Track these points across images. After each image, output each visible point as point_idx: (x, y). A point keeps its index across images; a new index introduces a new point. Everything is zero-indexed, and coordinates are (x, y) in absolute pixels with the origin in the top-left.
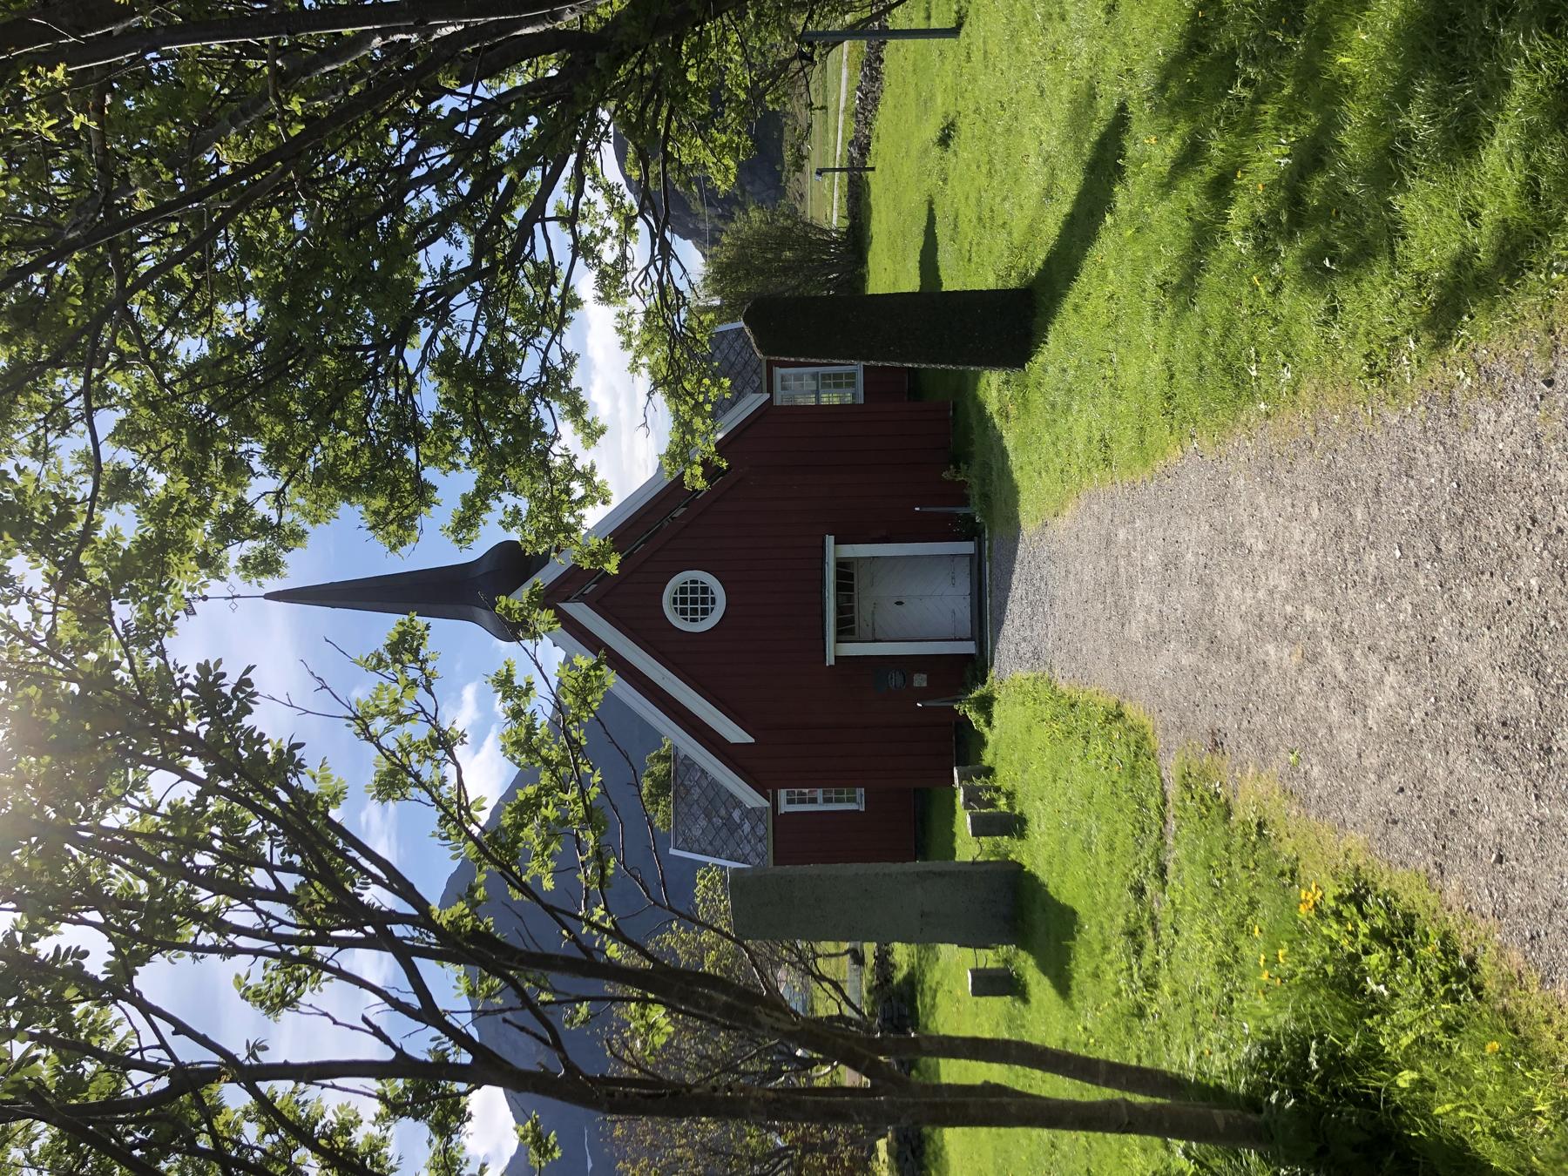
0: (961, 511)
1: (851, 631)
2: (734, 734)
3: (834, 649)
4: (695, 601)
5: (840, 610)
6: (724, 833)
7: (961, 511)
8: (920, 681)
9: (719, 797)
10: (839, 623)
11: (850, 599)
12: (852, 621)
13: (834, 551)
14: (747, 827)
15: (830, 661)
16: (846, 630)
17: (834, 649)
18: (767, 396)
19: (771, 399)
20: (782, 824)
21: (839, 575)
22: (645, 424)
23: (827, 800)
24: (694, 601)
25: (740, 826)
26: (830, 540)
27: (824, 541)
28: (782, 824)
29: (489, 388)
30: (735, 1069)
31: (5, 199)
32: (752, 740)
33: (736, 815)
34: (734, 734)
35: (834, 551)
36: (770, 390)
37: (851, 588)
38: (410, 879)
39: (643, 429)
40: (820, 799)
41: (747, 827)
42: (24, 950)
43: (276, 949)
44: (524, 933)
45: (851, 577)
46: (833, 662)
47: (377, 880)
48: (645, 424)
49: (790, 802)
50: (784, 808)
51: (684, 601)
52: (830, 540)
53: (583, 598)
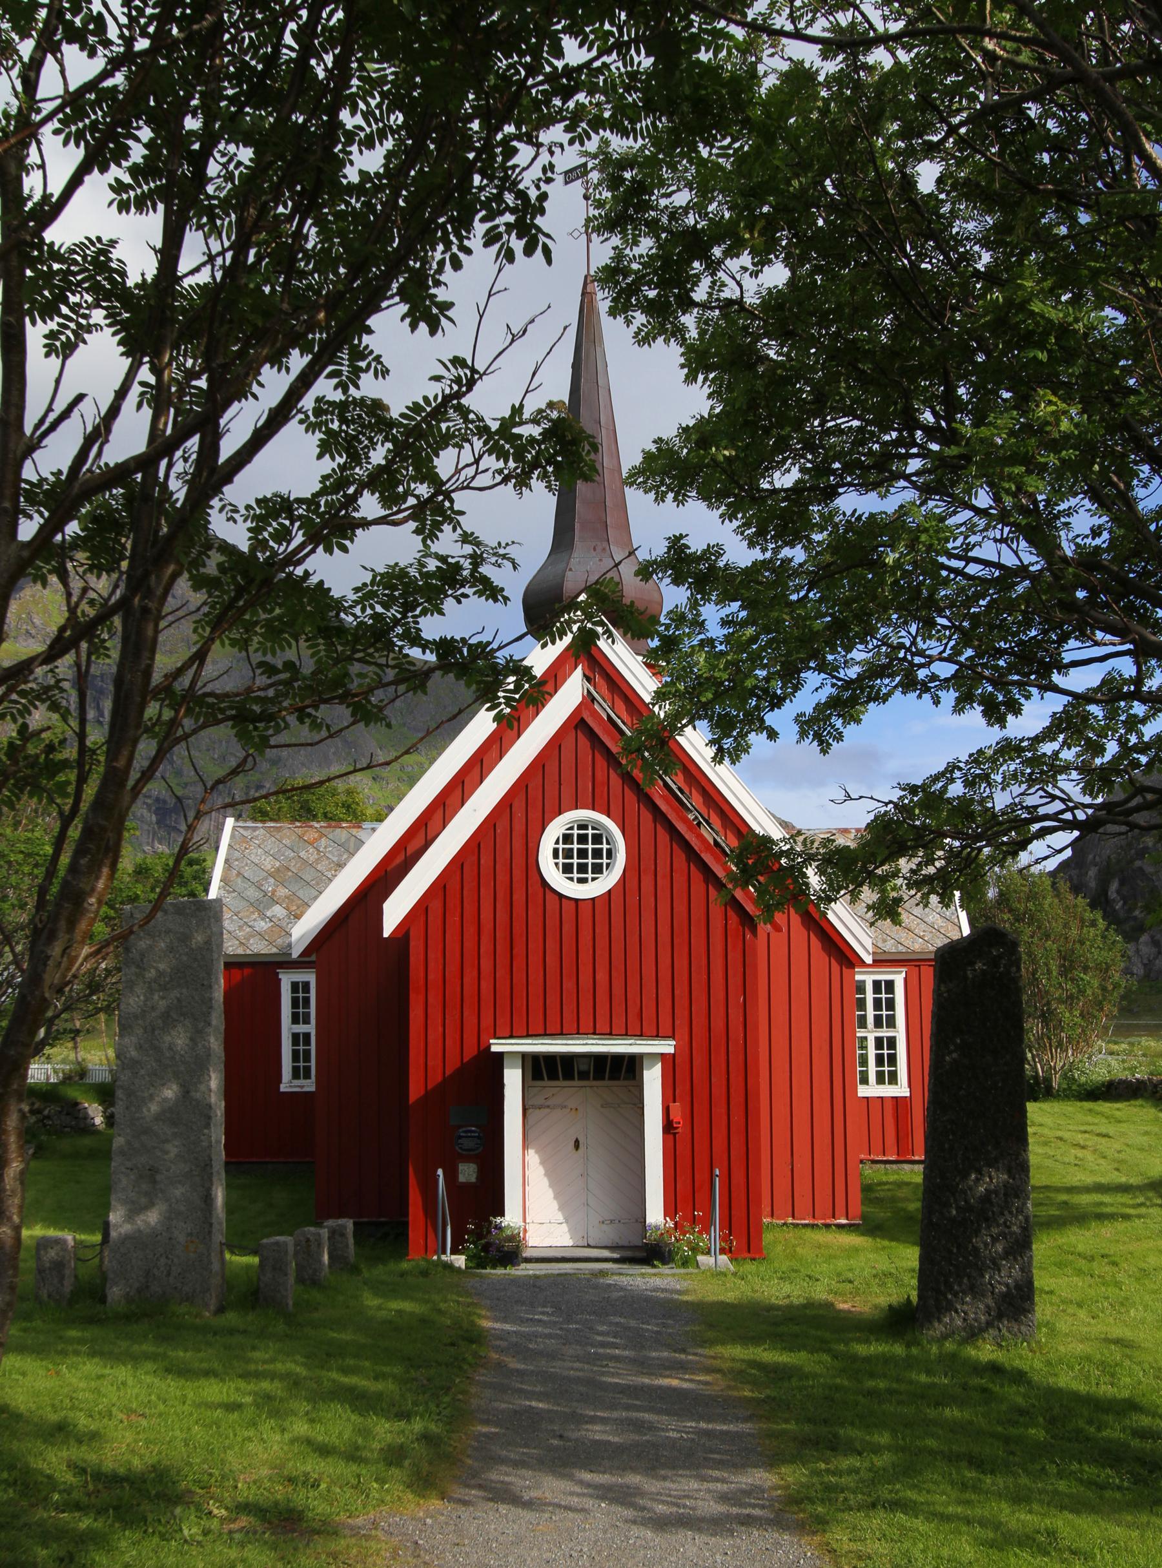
2: (395, 910)
4: (583, 855)
5: (568, 1060)
6: (252, 893)
8: (467, 1173)
10: (550, 1058)
11: (583, 1076)
12: (553, 1076)
14: (262, 925)
16: (539, 1069)
18: (869, 960)
19: (863, 963)
21: (618, 1059)
22: (849, 797)
24: (582, 854)
25: (263, 917)
26: (667, 1047)
29: (250, 605)
32: (386, 934)
33: (278, 911)
34: (395, 910)
36: (877, 963)
38: (237, 479)
39: (841, 796)
40: (301, 1028)
41: (262, 925)
43: (1052, 1195)
44: (180, 613)
46: (494, 1049)
48: (849, 797)
50: (286, 980)
51: (583, 839)
52: (667, 1047)
53: (589, 699)
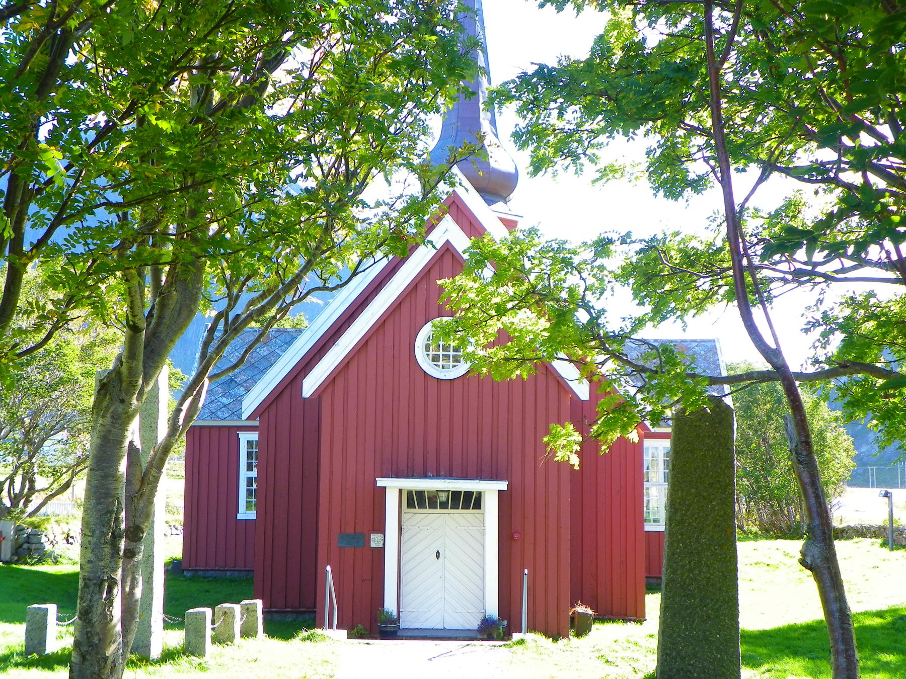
0: (81, 583)
1: (410, 505)
2: (310, 385)
3: (393, 487)
7: (81, 583)
9: (251, 365)
10: (420, 494)
11: (444, 505)
13: (490, 490)
15: (381, 482)
17: (393, 487)
20: (230, 434)
21: (468, 494)
23: (250, 481)
27: (502, 479)
28: (230, 434)
30: (788, 505)
31: (888, 31)
34: (310, 385)
35: (490, 490)
37: (455, 506)
42: (721, 19)
45: (466, 506)
47: (836, 272)
49: (250, 443)
52: (503, 485)
